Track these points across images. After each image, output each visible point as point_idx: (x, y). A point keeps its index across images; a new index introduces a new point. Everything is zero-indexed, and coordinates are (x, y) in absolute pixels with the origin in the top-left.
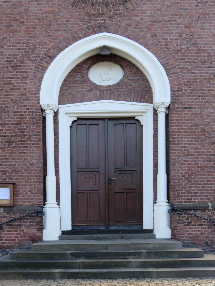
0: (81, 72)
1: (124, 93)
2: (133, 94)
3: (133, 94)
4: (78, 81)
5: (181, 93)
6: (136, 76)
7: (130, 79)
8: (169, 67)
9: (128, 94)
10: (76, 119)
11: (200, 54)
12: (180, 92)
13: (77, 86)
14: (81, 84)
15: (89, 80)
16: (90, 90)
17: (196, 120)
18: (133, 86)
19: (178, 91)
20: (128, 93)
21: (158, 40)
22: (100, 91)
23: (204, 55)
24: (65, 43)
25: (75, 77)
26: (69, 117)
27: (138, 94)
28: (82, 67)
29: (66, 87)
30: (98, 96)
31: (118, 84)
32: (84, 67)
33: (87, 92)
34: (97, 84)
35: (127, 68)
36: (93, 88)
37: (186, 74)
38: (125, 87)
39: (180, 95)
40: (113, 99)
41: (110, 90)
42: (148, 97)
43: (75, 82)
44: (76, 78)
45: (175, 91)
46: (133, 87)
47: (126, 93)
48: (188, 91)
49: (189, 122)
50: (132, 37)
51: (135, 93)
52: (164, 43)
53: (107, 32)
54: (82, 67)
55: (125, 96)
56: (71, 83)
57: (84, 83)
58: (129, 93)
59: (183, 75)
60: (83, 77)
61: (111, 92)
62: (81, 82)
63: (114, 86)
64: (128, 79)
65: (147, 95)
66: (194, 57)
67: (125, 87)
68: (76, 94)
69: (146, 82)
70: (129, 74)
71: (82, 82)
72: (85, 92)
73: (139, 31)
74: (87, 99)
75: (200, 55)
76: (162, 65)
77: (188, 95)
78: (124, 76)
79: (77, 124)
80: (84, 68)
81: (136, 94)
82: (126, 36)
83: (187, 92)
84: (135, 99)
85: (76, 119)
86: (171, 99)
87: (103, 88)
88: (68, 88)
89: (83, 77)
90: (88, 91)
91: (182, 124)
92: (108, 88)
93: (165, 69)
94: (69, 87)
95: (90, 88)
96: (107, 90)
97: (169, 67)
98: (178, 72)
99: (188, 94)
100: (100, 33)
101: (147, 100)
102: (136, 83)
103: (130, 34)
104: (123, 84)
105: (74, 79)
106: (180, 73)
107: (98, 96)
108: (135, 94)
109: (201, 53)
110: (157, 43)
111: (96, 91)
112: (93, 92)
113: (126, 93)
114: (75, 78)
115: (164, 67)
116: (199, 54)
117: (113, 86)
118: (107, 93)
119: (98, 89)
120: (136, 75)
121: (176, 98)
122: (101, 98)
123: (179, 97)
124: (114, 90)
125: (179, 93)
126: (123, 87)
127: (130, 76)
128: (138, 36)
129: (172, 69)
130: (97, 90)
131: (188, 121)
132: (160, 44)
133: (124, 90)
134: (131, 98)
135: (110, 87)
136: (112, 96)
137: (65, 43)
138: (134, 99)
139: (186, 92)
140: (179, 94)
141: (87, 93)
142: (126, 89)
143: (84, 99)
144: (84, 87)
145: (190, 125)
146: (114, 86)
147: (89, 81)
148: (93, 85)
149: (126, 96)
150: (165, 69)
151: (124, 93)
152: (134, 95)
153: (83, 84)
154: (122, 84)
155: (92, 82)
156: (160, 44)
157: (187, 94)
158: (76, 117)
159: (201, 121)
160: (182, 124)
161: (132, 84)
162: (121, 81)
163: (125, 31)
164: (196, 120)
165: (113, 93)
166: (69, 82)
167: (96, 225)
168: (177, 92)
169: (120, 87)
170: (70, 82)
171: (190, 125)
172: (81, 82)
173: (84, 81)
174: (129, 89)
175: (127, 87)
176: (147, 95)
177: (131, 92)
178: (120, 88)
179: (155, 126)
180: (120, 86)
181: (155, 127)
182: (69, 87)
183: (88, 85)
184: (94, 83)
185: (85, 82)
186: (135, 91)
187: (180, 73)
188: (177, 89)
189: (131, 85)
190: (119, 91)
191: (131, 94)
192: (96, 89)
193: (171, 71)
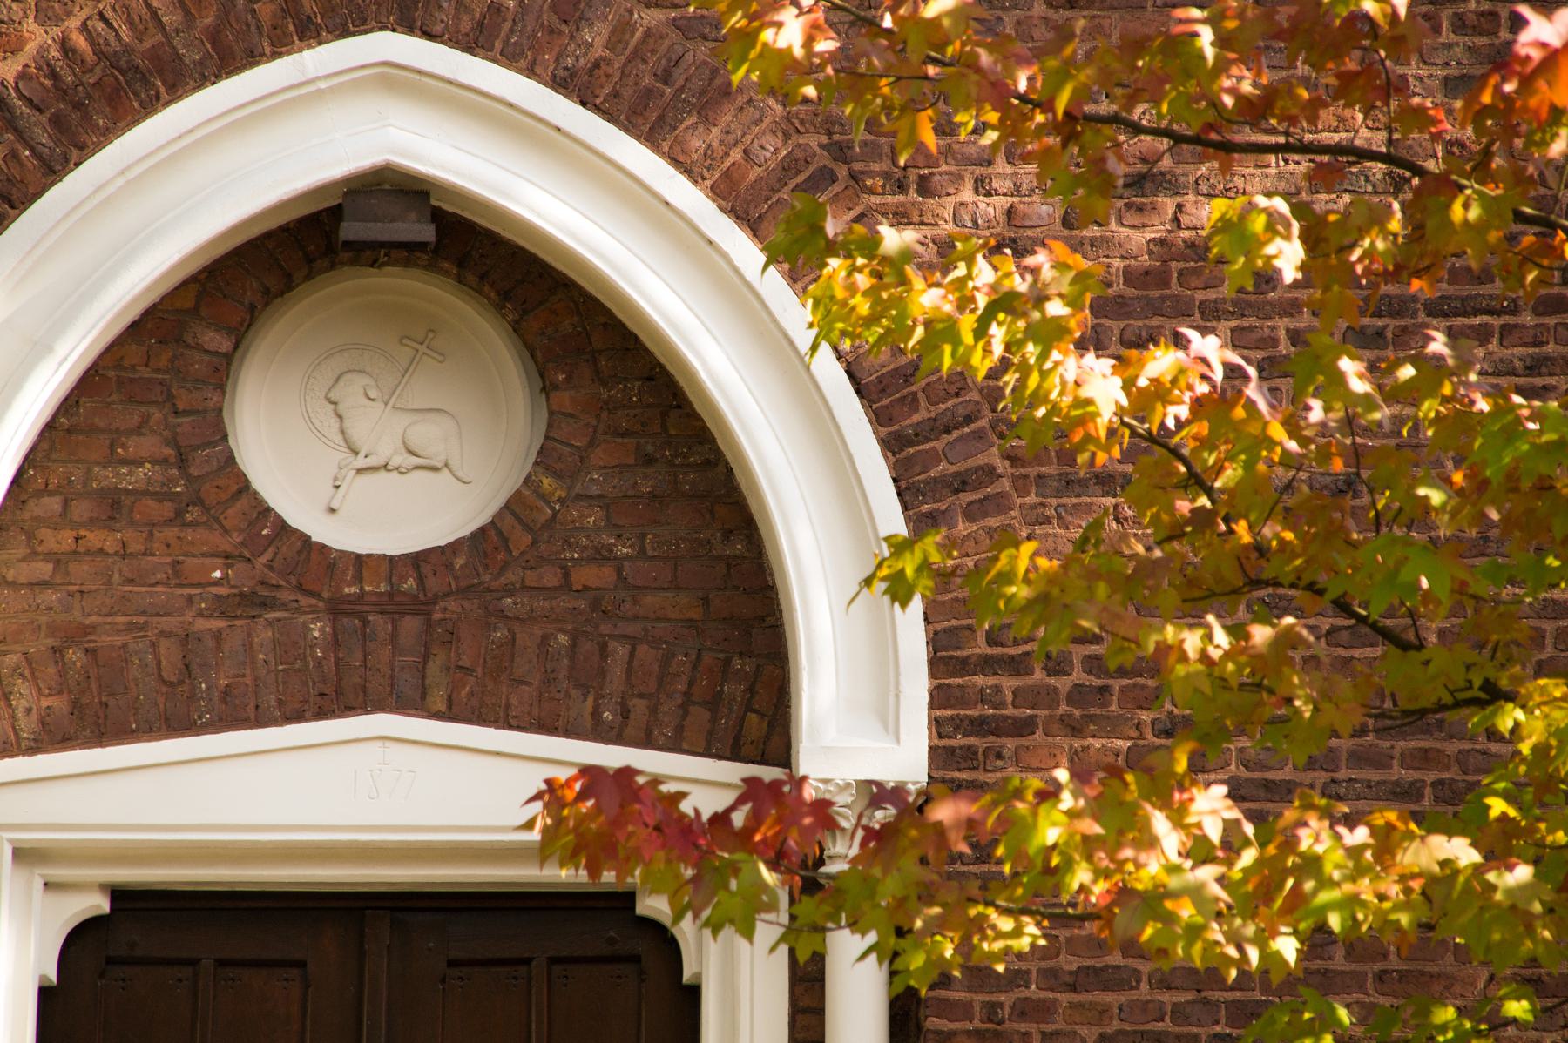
0: (170, 397)
1: (545, 640)
2: (620, 650)
3: (620, 650)
4: (146, 493)
5: (1016, 692)
6: (649, 461)
7: (595, 490)
8: (916, 418)
9: (574, 645)
10: (103, 905)
11: (1175, 288)
12: (1008, 684)
13: (136, 547)
14: (171, 533)
15: (244, 487)
16: (252, 603)
17: (1144, 986)
18: (619, 570)
19: (987, 665)
20: (575, 638)
21: (830, 134)
22: (337, 609)
23: (1211, 295)
24: (44, 119)
25: (112, 447)
26: (38, 884)
27: (666, 660)
28: (179, 340)
29: (33, 555)
30: (319, 663)
31: (483, 541)
32: (199, 348)
33: (221, 624)
34: (305, 539)
35: (568, 379)
36: (274, 579)
37: (1058, 493)
38: (551, 578)
39: (1010, 711)
40: (441, 706)
41: (421, 605)
42: (751, 690)
43: (116, 505)
44: (124, 462)
45: (965, 667)
46: (621, 578)
47: (563, 639)
48: (1078, 675)
49: (1081, 1005)
50: (616, 94)
51: (633, 642)
52: (876, 167)
53: (410, 29)
54: (179, 340)
55: (548, 681)
56: (81, 510)
57: (193, 524)
58: (587, 646)
59: (1032, 499)
60: (182, 462)
61: (429, 625)
62: (167, 510)
63: (459, 562)
64: (578, 488)
65: (737, 663)
66: (1128, 315)
67: (551, 578)
68: (118, 640)
69: (727, 534)
70: (592, 443)
71: (179, 513)
72: (200, 614)
73: (675, 36)
74: (216, 694)
75: (1176, 298)
76: (858, 391)
77: (1077, 713)
78: (545, 459)
79: (110, 961)
80: (196, 355)
81: (643, 650)
82: (562, 83)
83: (1063, 684)
84: (639, 706)
85: (103, 905)
86: (933, 750)
87: (358, 578)
88: (44, 569)
89: (182, 462)
90: (224, 615)
91: (1023, 1027)
92: (403, 579)
93: (884, 431)
94: (57, 560)
95: (243, 578)
96: (393, 605)
97: (916, 418)
98: (990, 473)
99: (1070, 700)
100: (345, 33)
101: (741, 721)
102: (643, 536)
103: (597, 65)
104: (534, 543)
105: (108, 477)
106: (1005, 485)
107: (319, 663)
108: (632, 655)
109: (1181, 273)
110: (824, 159)
111: (298, 610)
112: (270, 623)
113: (563, 638)
114: (112, 460)
115: (879, 418)
116: (1167, 285)
117: (449, 566)
118: (394, 637)
119: (317, 595)
120: (650, 449)
121: (972, 741)
122: (338, 692)
123: (997, 733)
124: (452, 605)
125: (997, 689)
126: (531, 578)
127: (599, 456)
128: (666, 78)
129: (947, 438)
130: (305, 601)
131: (1073, 988)
132: (842, 172)
133: (542, 604)
134: (599, 696)
135: (426, 569)
136: (434, 668)
137: (44, 119)
138: (625, 714)
139: (1052, 681)
140: (1003, 705)
141: (218, 636)
142: (564, 602)
143: (192, 698)
144: (191, 563)
145: (1096, 1031)
146: (459, 562)
147: (243, 503)
148: (271, 540)
149: (562, 675)
150: (884, 431)
151: (545, 640)
152: (629, 671)
153: (189, 535)
154: (528, 539)
155: (265, 511)
156: (842, 172)
157: (1064, 708)
158: (103, 887)
159: (1189, 996)
160: (1023, 1027)
161: (610, 548)
162: (513, 506)
163: (556, 22)
164: (1144, 986)
165: (451, 637)
166: (53, 504)
167: (164, 909)
168: (979, 680)
169: (511, 577)
170: (66, 503)
171: (1096, 1031)
172: (167, 510)
173: (198, 501)
174: (582, 604)
175: (567, 575)
176: (737, 663)
177: (605, 629)
178: (509, 591)
179: (804, 1011)
180: (504, 567)
181: (799, 1017)
182: (57, 560)
183: (225, 545)
184: (282, 527)
185: (207, 509)
186: (636, 618)
187: (1005, 485)
188: (981, 648)
189: (601, 556)
190: (502, 615)
191: (603, 647)
192: (300, 588)
193: (935, 457)
